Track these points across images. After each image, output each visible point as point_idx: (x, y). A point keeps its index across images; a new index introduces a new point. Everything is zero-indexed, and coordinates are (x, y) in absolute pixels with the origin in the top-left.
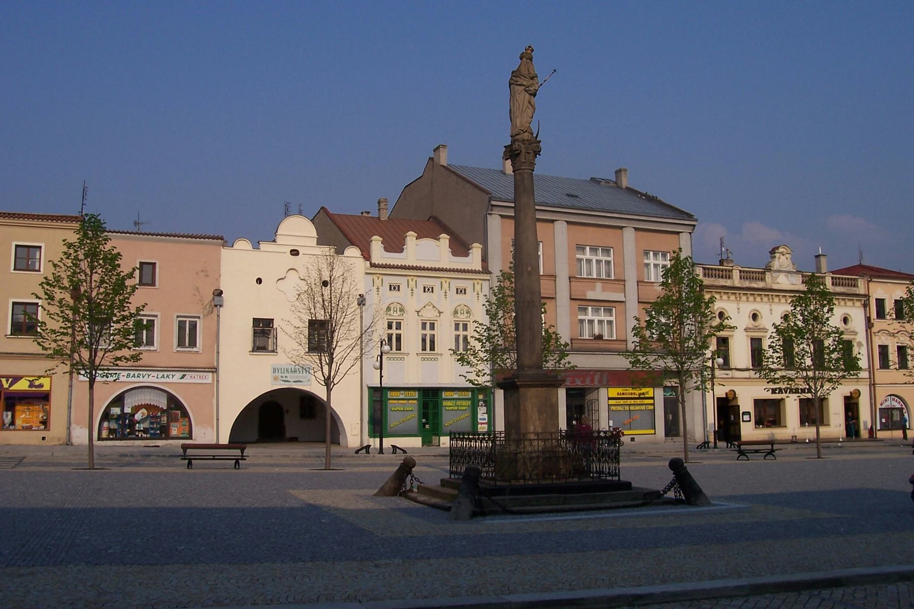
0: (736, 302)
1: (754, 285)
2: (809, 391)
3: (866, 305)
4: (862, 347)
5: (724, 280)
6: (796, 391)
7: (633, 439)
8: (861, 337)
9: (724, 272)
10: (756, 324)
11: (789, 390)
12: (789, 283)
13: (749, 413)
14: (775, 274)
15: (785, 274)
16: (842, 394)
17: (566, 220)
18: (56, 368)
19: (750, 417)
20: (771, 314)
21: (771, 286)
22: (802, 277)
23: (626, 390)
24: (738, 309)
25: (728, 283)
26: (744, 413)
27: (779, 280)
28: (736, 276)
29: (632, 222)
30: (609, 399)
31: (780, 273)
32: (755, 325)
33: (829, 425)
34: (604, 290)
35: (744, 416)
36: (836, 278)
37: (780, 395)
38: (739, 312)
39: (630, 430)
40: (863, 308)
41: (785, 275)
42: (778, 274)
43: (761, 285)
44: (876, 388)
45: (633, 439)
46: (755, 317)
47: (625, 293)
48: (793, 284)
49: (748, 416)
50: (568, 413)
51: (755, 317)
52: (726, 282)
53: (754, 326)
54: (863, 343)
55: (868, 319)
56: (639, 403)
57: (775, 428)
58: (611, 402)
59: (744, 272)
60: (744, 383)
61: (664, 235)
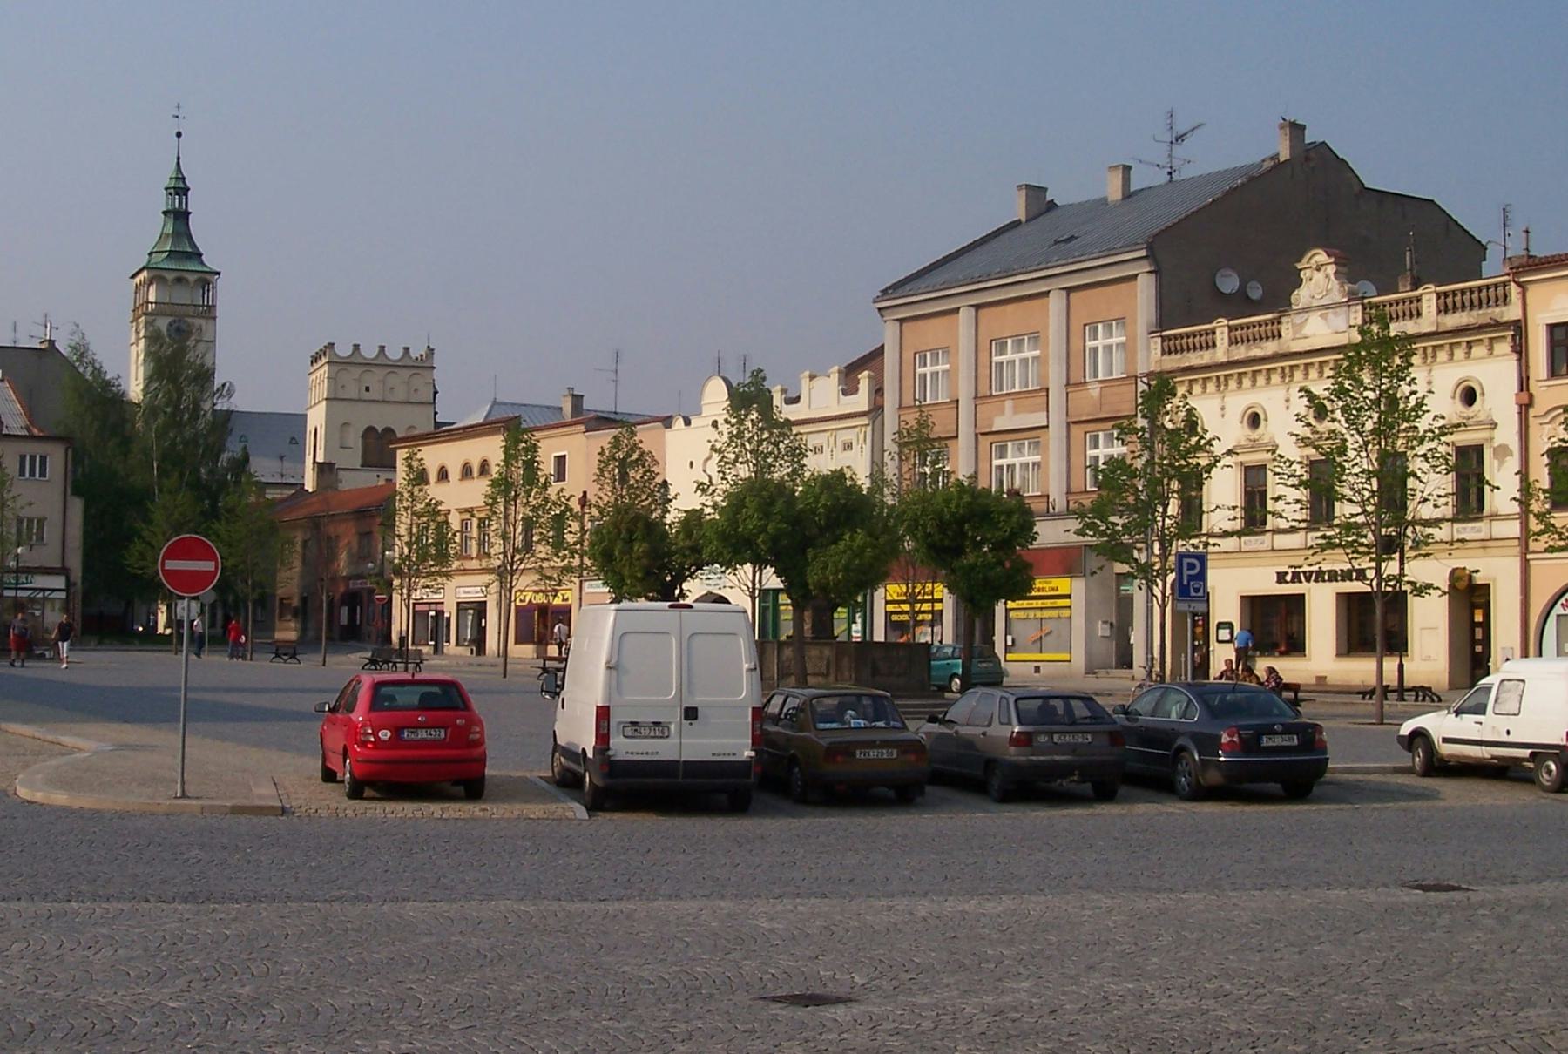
0: (1424, 368)
1: (1256, 352)
2: (1361, 574)
3: (1520, 350)
4: (1508, 458)
5: (1199, 353)
6: (1333, 576)
7: (1037, 669)
8: (1507, 433)
9: (1492, 290)
10: (1255, 435)
11: (1314, 575)
12: (1329, 331)
13: (1230, 626)
14: (1298, 319)
15: (1319, 313)
16: (1494, 580)
17: (896, 317)
18: (1098, 571)
19: (1232, 634)
20: (1288, 408)
21: (1288, 347)
22: (1364, 309)
23: (1046, 583)
24: (1223, 409)
25: (1205, 358)
26: (1220, 625)
27: (1307, 331)
28: (1429, 307)
29: (1025, 285)
30: (887, 602)
31: (1310, 314)
32: (1252, 438)
33: (1558, 656)
34: (1016, 411)
35: (1221, 631)
36: (1446, 294)
37: (1297, 585)
38: (1223, 416)
39: (1041, 652)
40: (1515, 356)
41: (1321, 316)
42: (1306, 315)
43: (1270, 347)
44: (1532, 563)
45: (1037, 669)
46: (1254, 420)
47: (1048, 411)
48: (1337, 333)
49: (1228, 631)
50: (991, 627)
51: (1254, 420)
52: (1202, 356)
53: (1464, 418)
54: (1511, 447)
55: (1524, 383)
56: (1049, 605)
57: (1281, 658)
58: (890, 608)
59: (1236, 328)
60: (1232, 563)
61: (926, 321)
